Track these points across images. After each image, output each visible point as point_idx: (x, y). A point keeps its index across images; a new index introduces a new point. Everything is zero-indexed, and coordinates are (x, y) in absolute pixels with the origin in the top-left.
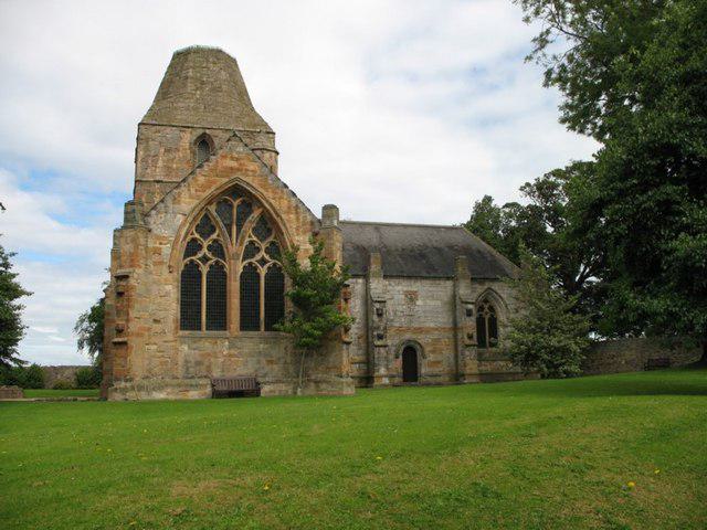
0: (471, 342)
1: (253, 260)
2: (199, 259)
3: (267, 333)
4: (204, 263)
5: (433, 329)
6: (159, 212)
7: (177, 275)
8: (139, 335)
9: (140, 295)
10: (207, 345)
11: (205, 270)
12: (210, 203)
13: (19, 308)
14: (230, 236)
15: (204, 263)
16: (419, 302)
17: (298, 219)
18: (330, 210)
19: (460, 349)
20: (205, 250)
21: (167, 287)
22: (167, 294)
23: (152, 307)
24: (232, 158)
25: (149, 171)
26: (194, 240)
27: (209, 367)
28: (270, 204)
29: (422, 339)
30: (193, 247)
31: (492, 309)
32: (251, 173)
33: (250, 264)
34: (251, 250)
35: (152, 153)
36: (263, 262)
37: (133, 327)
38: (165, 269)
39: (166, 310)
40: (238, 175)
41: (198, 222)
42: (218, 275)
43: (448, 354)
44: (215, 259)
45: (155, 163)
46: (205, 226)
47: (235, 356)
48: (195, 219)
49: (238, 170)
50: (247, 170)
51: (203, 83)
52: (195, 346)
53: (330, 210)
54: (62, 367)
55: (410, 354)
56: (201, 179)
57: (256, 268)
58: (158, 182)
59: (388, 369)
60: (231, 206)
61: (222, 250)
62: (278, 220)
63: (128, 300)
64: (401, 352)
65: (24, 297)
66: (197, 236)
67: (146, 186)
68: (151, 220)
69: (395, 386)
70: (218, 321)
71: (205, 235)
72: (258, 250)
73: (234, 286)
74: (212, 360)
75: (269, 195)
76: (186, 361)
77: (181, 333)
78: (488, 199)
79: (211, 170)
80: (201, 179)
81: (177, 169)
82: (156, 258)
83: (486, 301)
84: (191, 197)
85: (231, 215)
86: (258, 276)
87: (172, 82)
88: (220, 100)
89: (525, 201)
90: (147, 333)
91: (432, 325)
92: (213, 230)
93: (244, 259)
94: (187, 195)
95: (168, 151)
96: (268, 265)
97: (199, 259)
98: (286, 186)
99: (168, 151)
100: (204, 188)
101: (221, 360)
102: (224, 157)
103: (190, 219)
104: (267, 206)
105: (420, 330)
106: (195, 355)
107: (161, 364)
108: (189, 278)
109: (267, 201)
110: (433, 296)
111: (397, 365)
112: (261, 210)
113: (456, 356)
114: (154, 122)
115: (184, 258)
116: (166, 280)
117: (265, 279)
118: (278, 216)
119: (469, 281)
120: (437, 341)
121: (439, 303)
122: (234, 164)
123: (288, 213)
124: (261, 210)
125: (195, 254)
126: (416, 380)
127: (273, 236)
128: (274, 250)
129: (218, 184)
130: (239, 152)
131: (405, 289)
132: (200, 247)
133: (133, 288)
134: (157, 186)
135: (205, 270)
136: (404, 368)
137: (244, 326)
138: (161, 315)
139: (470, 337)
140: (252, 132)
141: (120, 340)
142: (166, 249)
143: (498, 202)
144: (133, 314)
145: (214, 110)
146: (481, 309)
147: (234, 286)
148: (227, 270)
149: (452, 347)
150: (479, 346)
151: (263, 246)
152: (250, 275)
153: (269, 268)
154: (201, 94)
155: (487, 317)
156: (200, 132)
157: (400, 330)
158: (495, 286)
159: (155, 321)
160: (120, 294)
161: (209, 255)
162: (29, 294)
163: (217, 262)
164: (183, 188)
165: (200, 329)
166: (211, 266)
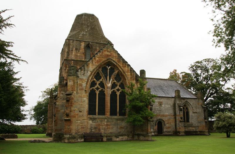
0: (182, 120)
1: (115, 89)
2: (96, 88)
3: (120, 117)
4: (97, 90)
5: (168, 115)
7: (88, 94)
8: (74, 117)
9: (75, 101)
12: (99, 68)
16: (163, 106)
17: (131, 74)
18: (143, 72)
19: (177, 122)
20: (98, 85)
21: (84, 98)
22: (84, 101)
23: (147, 113)
24: (108, 51)
26: (94, 81)
28: (122, 69)
29: (164, 119)
30: (93, 84)
31: (187, 108)
32: (114, 57)
33: (114, 91)
37: (72, 114)
38: (84, 92)
39: (84, 107)
40: (110, 57)
41: (95, 74)
42: (102, 94)
43: (173, 124)
44: (121, 90)
46: (97, 76)
47: (109, 125)
48: (94, 73)
50: (113, 56)
51: (88, 26)
52: (95, 121)
53: (143, 72)
54: (26, 126)
55: (160, 124)
56: (97, 59)
57: (95, 91)
58: (73, 60)
59: (153, 129)
60: (107, 69)
61: (104, 85)
62: (125, 74)
63: (71, 103)
64: (157, 123)
66: (95, 80)
68: (79, 73)
70: (102, 112)
71: (98, 80)
72: (116, 85)
73: (108, 99)
77: (89, 116)
78: (176, 71)
79: (100, 55)
81: (80, 56)
82: (81, 87)
83: (185, 106)
85: (107, 72)
86: (116, 95)
90: (77, 116)
91: (167, 114)
92: (101, 78)
96: (99, 90)
97: (96, 88)
103: (93, 73)
104: (120, 69)
105: (163, 116)
107: (82, 128)
108: (92, 96)
109: (121, 67)
110: (167, 104)
111: (156, 127)
112: (118, 70)
113: (176, 125)
115: (111, 89)
116: (84, 96)
117: (119, 97)
121: (170, 106)
122: (109, 54)
123: (128, 72)
124: (118, 70)
126: (34, 110)
128: (122, 86)
131: (158, 101)
132: (96, 84)
133: (73, 99)
134: (73, 62)
136: (158, 129)
137: (111, 114)
138: (82, 109)
139: (181, 118)
141: (68, 119)
143: (178, 72)
144: (72, 109)
146: (184, 108)
147: (108, 99)
148: (106, 93)
149: (174, 122)
150: (184, 122)
151: (118, 84)
152: (113, 95)
153: (120, 92)
155: (185, 111)
156: (87, 43)
157: (157, 116)
159: (80, 111)
160: (68, 101)
161: (99, 87)
163: (102, 90)
164: (90, 61)
166: (100, 91)
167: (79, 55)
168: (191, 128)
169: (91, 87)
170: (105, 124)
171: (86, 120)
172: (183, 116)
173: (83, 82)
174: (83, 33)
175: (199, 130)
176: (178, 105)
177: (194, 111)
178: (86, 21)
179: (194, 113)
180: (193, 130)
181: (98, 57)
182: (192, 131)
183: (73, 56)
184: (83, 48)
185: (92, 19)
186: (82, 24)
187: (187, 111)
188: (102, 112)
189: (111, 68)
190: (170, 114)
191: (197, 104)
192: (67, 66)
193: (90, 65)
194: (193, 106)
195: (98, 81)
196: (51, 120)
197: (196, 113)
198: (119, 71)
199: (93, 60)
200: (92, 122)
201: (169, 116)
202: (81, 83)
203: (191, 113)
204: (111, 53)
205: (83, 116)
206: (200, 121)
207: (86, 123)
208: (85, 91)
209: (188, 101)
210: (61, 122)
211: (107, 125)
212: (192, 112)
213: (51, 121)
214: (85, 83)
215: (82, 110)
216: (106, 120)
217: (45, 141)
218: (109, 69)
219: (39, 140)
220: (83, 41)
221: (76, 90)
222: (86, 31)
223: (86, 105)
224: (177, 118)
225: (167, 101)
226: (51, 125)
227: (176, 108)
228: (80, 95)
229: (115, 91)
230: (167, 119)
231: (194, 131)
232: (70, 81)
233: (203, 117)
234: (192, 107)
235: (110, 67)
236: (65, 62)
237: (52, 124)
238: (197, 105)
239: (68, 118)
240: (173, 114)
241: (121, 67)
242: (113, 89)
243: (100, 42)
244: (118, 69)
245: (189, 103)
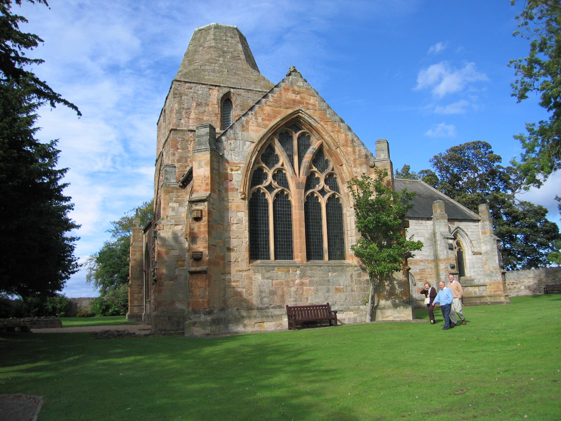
3: (332, 262)
6: (228, 139)
10: (280, 274)
13: (73, 239)
14: (293, 165)
17: (354, 152)
24: (294, 92)
25: (182, 121)
27: (283, 296)
34: (311, 181)
35: (186, 106)
36: (323, 192)
41: (264, 151)
42: (282, 201)
45: (188, 113)
49: (300, 103)
50: (307, 103)
51: (224, 52)
52: (268, 275)
56: (267, 109)
65: (74, 230)
67: (179, 135)
69: (535, 296)
74: (285, 289)
76: (261, 292)
79: (275, 101)
80: (267, 109)
84: (258, 125)
86: (319, 205)
87: (195, 51)
88: (240, 66)
89: (99, 289)
94: (255, 124)
95: (199, 105)
96: (276, 191)
98: (342, 121)
99: (199, 105)
100: (270, 117)
102: (287, 90)
106: (267, 285)
109: (327, 133)
114: (187, 80)
116: (238, 207)
119: (446, 221)
120: (423, 270)
122: (298, 98)
123: (346, 145)
130: (299, 87)
141: (198, 269)
145: (235, 73)
154: (224, 61)
156: (226, 90)
158: (462, 225)
162: (78, 227)
164: (250, 116)
165: (321, 257)
168: (470, 289)
171: (245, 273)
172: (455, 261)
173: (234, 168)
174: (212, 68)
175: (489, 294)
176: (442, 235)
177: (476, 251)
178: (218, 41)
179: (475, 254)
180: (475, 293)
181: (269, 106)
182: (473, 295)
183: (191, 121)
184: (215, 102)
187: (459, 249)
188: (285, 251)
190: (425, 258)
191: (480, 233)
192: (179, 146)
193: (252, 127)
194: (472, 239)
196: (140, 282)
197: (480, 254)
198: (324, 143)
199: (256, 113)
200: (263, 278)
201: (422, 264)
203: (468, 258)
204: (302, 95)
205: (238, 262)
206: (489, 272)
207: (246, 281)
209: (461, 227)
210: (172, 282)
211: (302, 284)
212: (470, 252)
213: (139, 285)
214: (239, 172)
215: (235, 245)
216: (298, 272)
217: (135, 333)
219: (118, 331)
220: (216, 86)
221: (217, 191)
222: (221, 62)
223: (243, 232)
224: (442, 266)
225: (416, 227)
226: (138, 293)
227: (438, 242)
229: (315, 195)
230: (418, 270)
231: (478, 294)
232: (199, 164)
233: (497, 262)
234: (471, 242)
236: (171, 136)
237: (140, 292)
238: (481, 236)
239: (198, 266)
240: (432, 258)
241: (327, 133)
242: (311, 188)
243: (255, 89)
245: (463, 231)
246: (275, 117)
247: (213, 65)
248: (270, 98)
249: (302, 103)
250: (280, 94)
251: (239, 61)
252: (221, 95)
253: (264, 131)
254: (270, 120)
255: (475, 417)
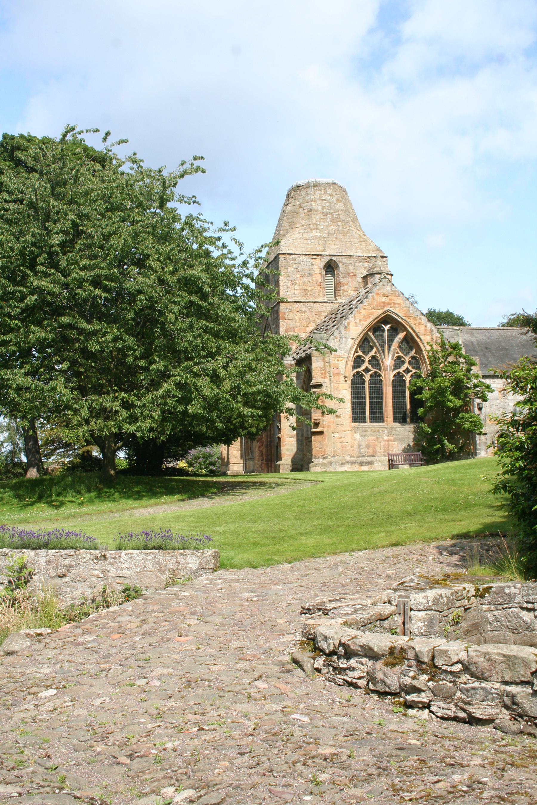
2: (363, 371)
7: (349, 383)
11: (367, 377)
14: (383, 352)
15: (407, 374)
21: (344, 391)
24: (384, 295)
30: (358, 361)
34: (399, 362)
44: (414, 371)
49: (388, 304)
50: (394, 304)
56: (363, 312)
57: (362, 375)
60: (383, 330)
61: (379, 364)
62: (418, 340)
70: (377, 415)
71: (366, 353)
75: (411, 322)
76: (359, 445)
82: (336, 371)
86: (404, 381)
92: (372, 348)
93: (394, 369)
101: (383, 443)
107: (342, 446)
108: (357, 383)
112: (405, 333)
118: (418, 337)
122: (386, 300)
124: (405, 333)
125: (359, 367)
127: (414, 351)
129: (375, 315)
135: (367, 377)
140: (369, 257)
142: (342, 365)
151: (407, 359)
152: (398, 380)
153: (371, 376)
156: (327, 258)
167: (309, 288)
169: (354, 368)
170: (386, 438)
173: (340, 359)
185: (331, 195)
186: (311, 210)
189: (391, 327)
195: (366, 355)
200: (361, 436)
202: (336, 361)
208: (345, 377)
218: (388, 330)
222: (322, 227)
228: (336, 385)
235: (389, 326)
244: (405, 329)
246: (369, 317)
247: (314, 231)
248: (365, 302)
249: (391, 304)
250: (374, 299)
251: (339, 224)
252: (324, 264)
253: (361, 329)
254: (366, 321)
255: (308, 694)
